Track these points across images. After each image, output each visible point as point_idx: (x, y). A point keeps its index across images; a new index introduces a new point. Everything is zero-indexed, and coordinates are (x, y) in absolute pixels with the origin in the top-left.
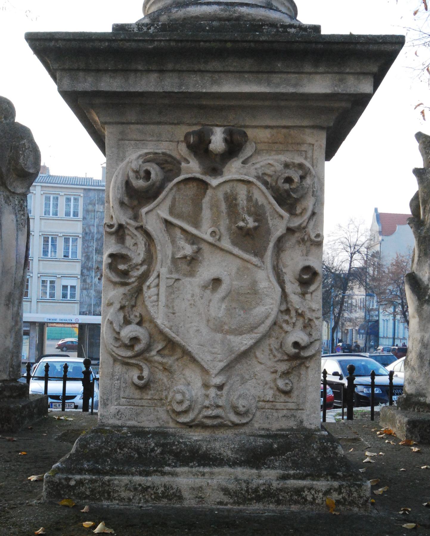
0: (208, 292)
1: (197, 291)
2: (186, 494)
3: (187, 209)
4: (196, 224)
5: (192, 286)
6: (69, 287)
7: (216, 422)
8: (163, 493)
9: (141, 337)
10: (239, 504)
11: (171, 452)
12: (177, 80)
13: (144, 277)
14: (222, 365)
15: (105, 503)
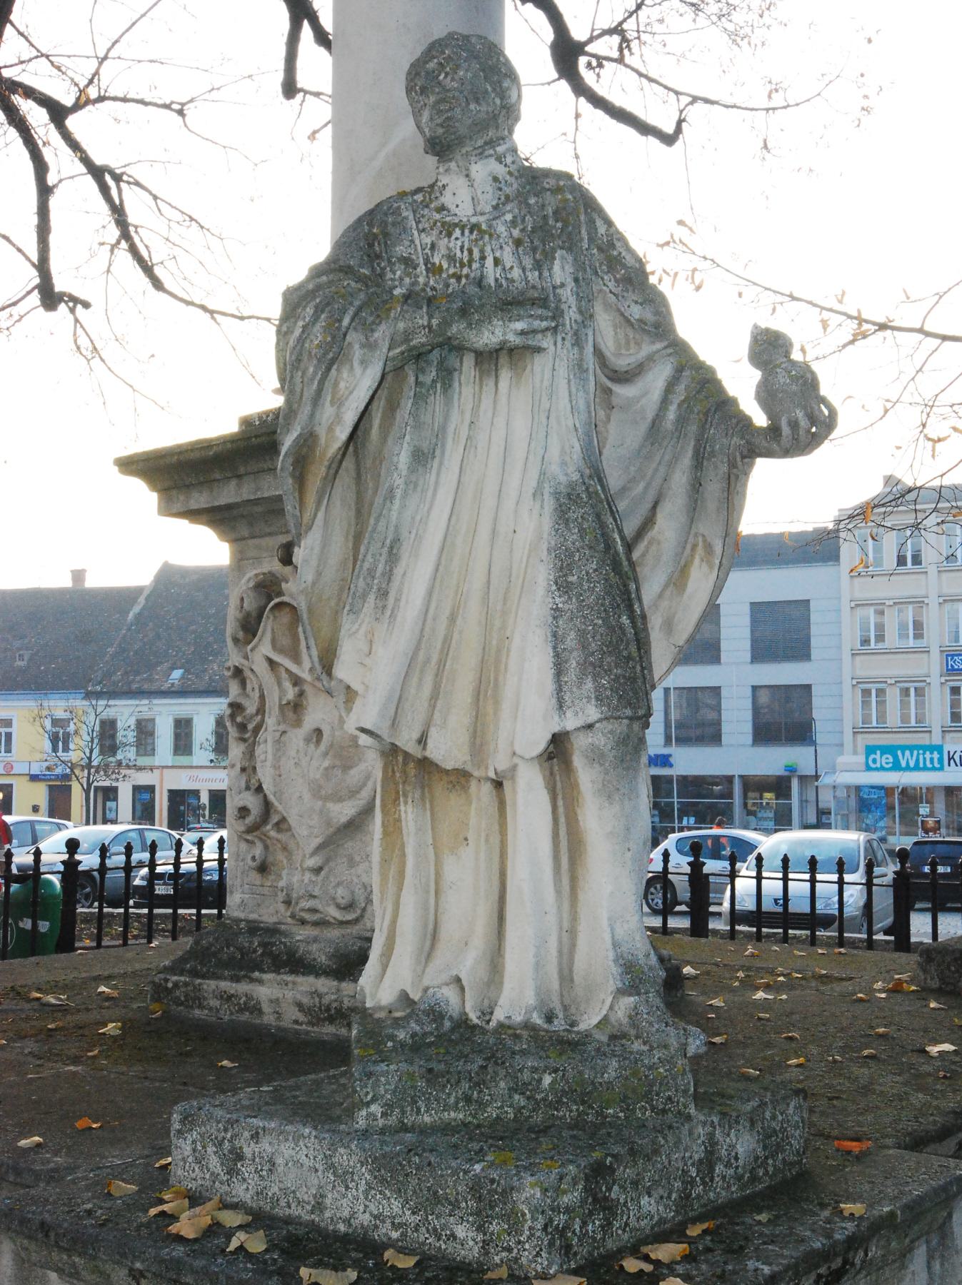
0: (312, 746)
1: (301, 743)
2: (266, 1008)
3: (285, 641)
4: (296, 658)
5: (297, 738)
6: (737, 788)
7: (316, 917)
8: (245, 1003)
9: (250, 806)
10: (313, 1025)
11: (271, 954)
12: (253, 485)
13: (257, 730)
14: (317, 842)
15: (197, 1012)
